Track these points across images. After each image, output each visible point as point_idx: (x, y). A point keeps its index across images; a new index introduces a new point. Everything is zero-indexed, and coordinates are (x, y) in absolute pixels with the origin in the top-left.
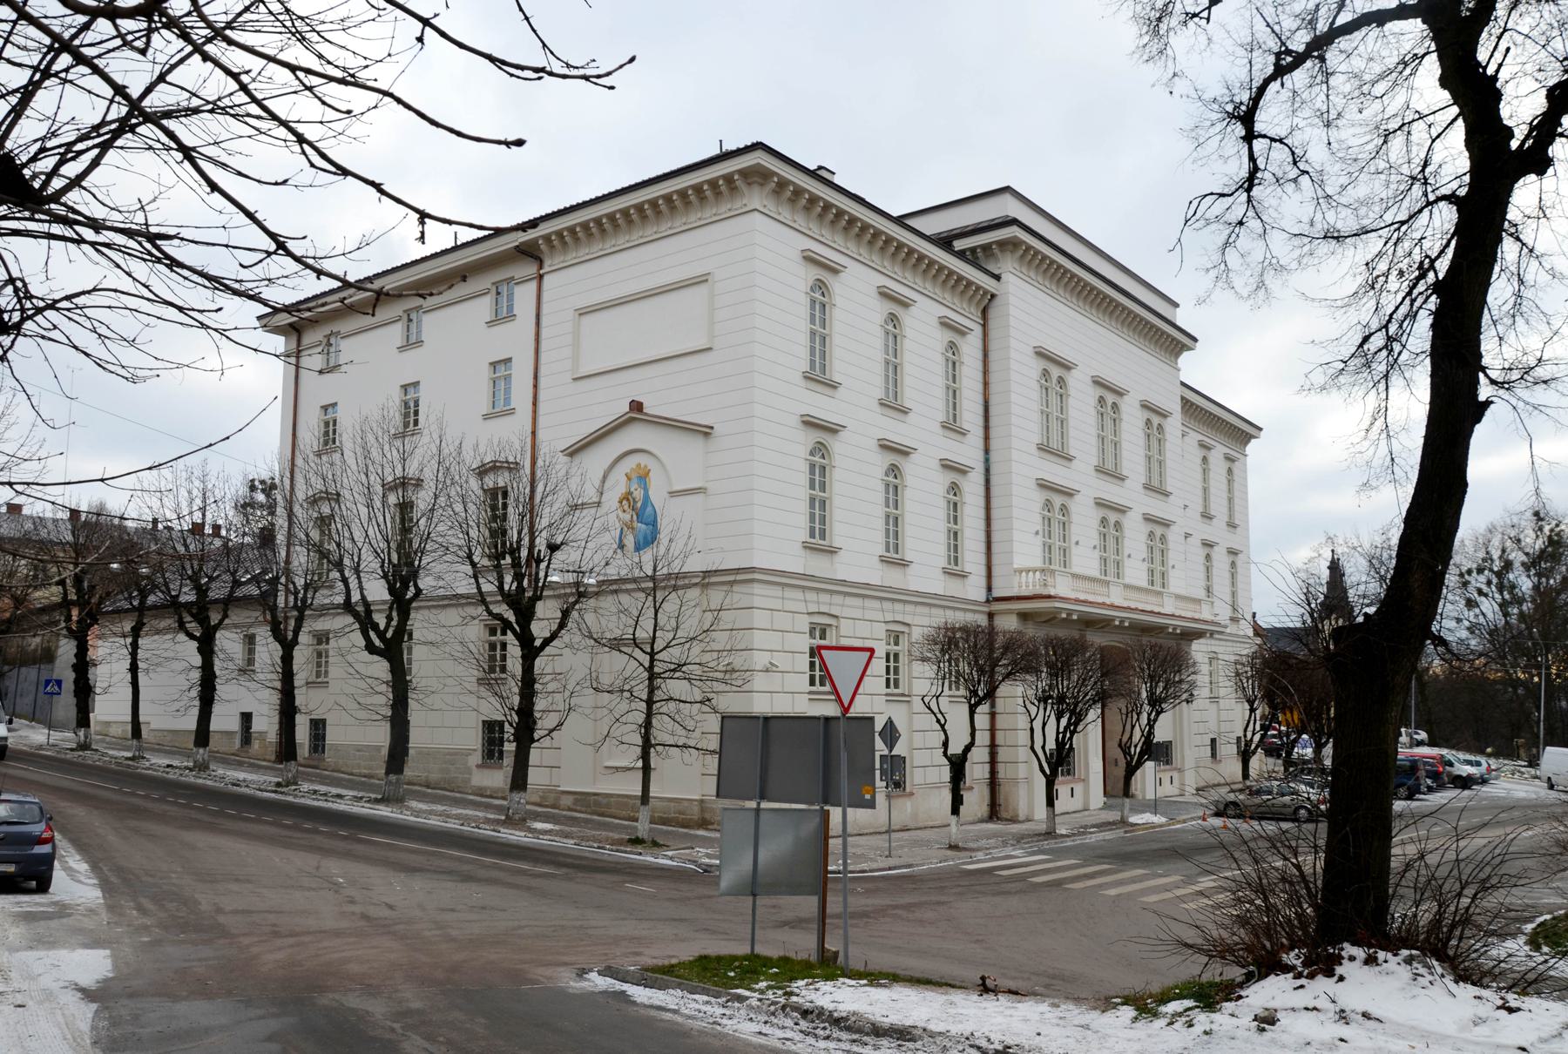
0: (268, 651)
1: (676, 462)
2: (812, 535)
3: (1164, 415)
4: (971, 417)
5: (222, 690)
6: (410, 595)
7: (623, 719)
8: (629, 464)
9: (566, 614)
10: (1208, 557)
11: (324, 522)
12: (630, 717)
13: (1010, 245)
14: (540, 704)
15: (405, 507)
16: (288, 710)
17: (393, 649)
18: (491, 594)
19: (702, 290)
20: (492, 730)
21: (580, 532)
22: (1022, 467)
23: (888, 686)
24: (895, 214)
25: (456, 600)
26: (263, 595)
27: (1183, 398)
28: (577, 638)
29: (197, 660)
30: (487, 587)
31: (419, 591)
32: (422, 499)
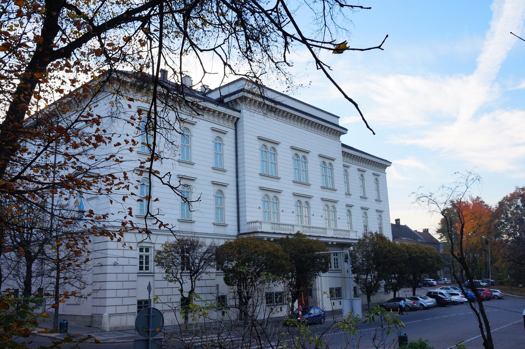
4: (229, 163)
27: (343, 152)
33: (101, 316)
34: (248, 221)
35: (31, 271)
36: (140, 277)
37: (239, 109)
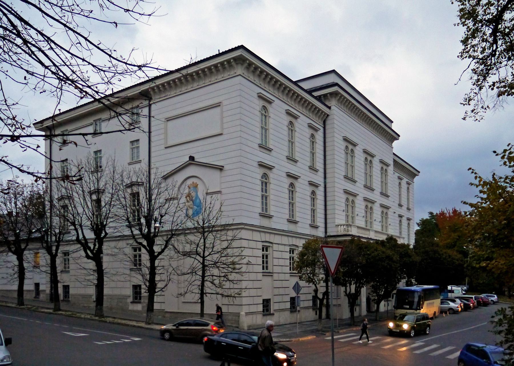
0: (44, 258)
1: (210, 180)
2: (263, 210)
3: (387, 165)
4: (319, 165)
5: (27, 275)
6: (103, 235)
7: (193, 284)
8: (189, 182)
9: (167, 242)
10: (400, 221)
11: (65, 207)
12: (196, 283)
13: (335, 94)
14: (157, 278)
15: (98, 201)
16: (54, 281)
17: (97, 257)
18: (137, 235)
19: (217, 110)
20: (137, 288)
21: (172, 209)
22: (338, 185)
23: (263, 269)
24: (294, 80)
25: (123, 238)
26: (42, 237)
28: (173, 253)
29: (17, 263)
30: (136, 232)
31: (106, 234)
32: (105, 198)
33: (238, 315)
34: (336, 224)
35: (24, 268)
36: (265, 277)
37: (329, 105)
